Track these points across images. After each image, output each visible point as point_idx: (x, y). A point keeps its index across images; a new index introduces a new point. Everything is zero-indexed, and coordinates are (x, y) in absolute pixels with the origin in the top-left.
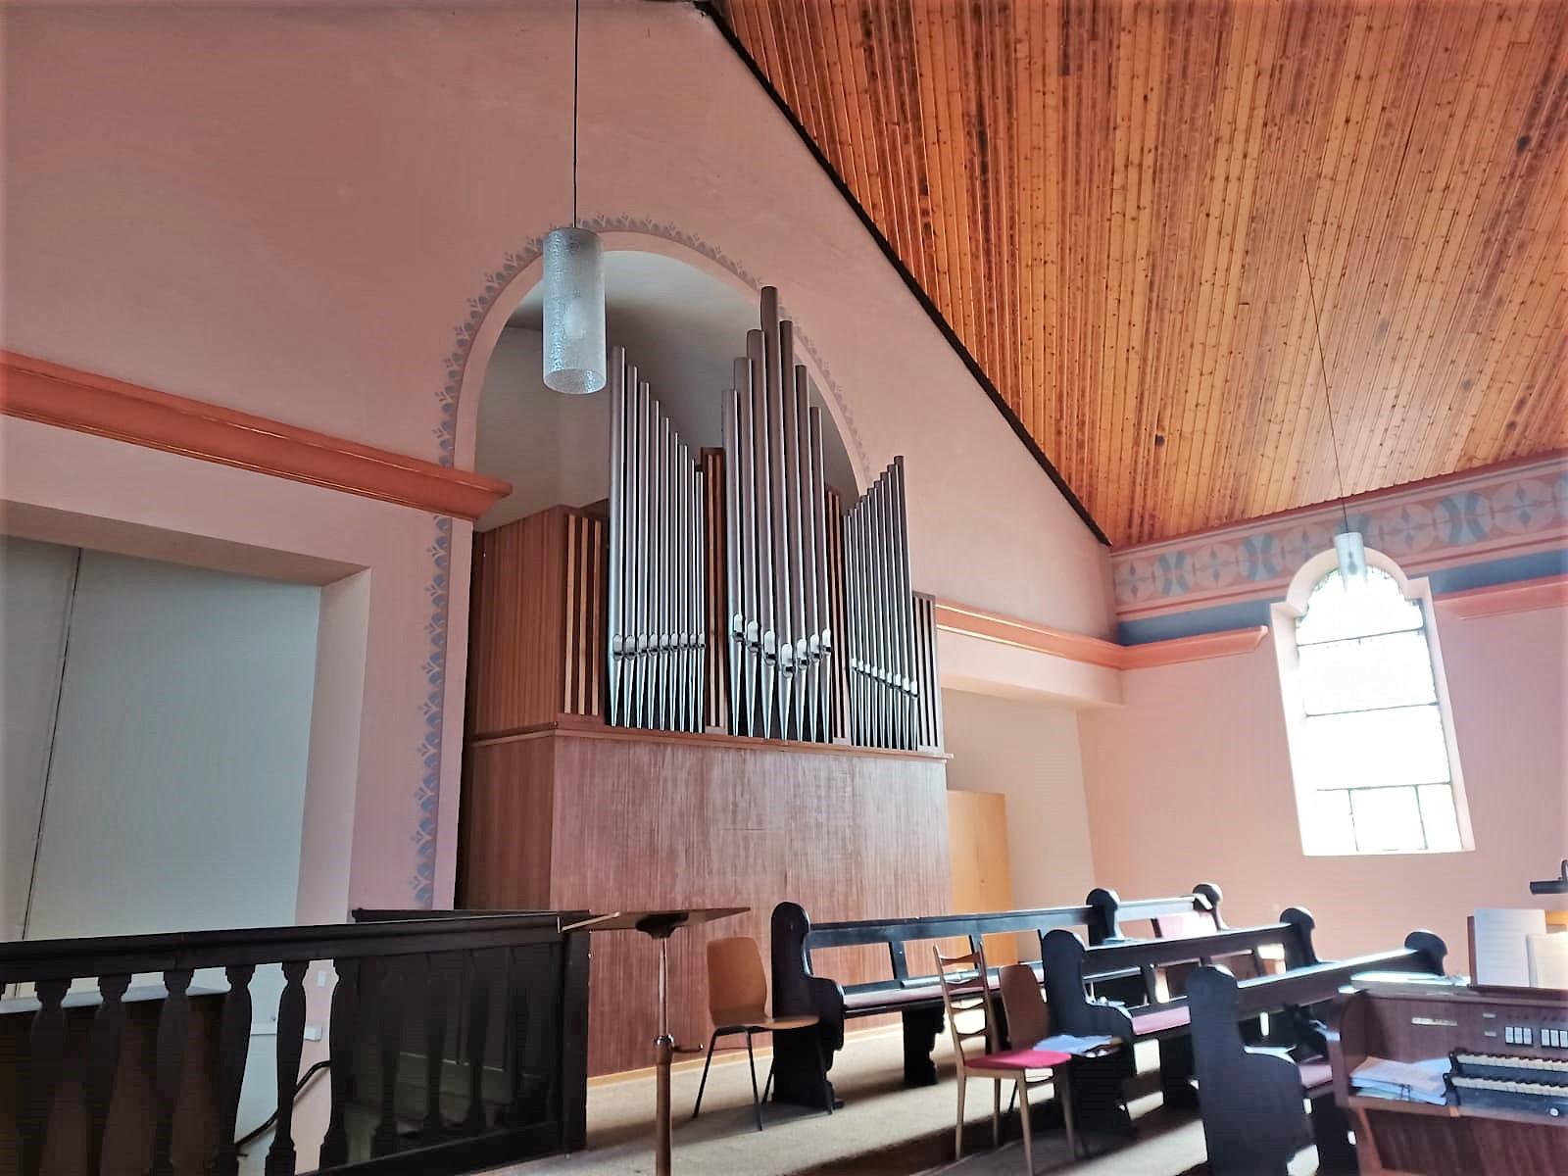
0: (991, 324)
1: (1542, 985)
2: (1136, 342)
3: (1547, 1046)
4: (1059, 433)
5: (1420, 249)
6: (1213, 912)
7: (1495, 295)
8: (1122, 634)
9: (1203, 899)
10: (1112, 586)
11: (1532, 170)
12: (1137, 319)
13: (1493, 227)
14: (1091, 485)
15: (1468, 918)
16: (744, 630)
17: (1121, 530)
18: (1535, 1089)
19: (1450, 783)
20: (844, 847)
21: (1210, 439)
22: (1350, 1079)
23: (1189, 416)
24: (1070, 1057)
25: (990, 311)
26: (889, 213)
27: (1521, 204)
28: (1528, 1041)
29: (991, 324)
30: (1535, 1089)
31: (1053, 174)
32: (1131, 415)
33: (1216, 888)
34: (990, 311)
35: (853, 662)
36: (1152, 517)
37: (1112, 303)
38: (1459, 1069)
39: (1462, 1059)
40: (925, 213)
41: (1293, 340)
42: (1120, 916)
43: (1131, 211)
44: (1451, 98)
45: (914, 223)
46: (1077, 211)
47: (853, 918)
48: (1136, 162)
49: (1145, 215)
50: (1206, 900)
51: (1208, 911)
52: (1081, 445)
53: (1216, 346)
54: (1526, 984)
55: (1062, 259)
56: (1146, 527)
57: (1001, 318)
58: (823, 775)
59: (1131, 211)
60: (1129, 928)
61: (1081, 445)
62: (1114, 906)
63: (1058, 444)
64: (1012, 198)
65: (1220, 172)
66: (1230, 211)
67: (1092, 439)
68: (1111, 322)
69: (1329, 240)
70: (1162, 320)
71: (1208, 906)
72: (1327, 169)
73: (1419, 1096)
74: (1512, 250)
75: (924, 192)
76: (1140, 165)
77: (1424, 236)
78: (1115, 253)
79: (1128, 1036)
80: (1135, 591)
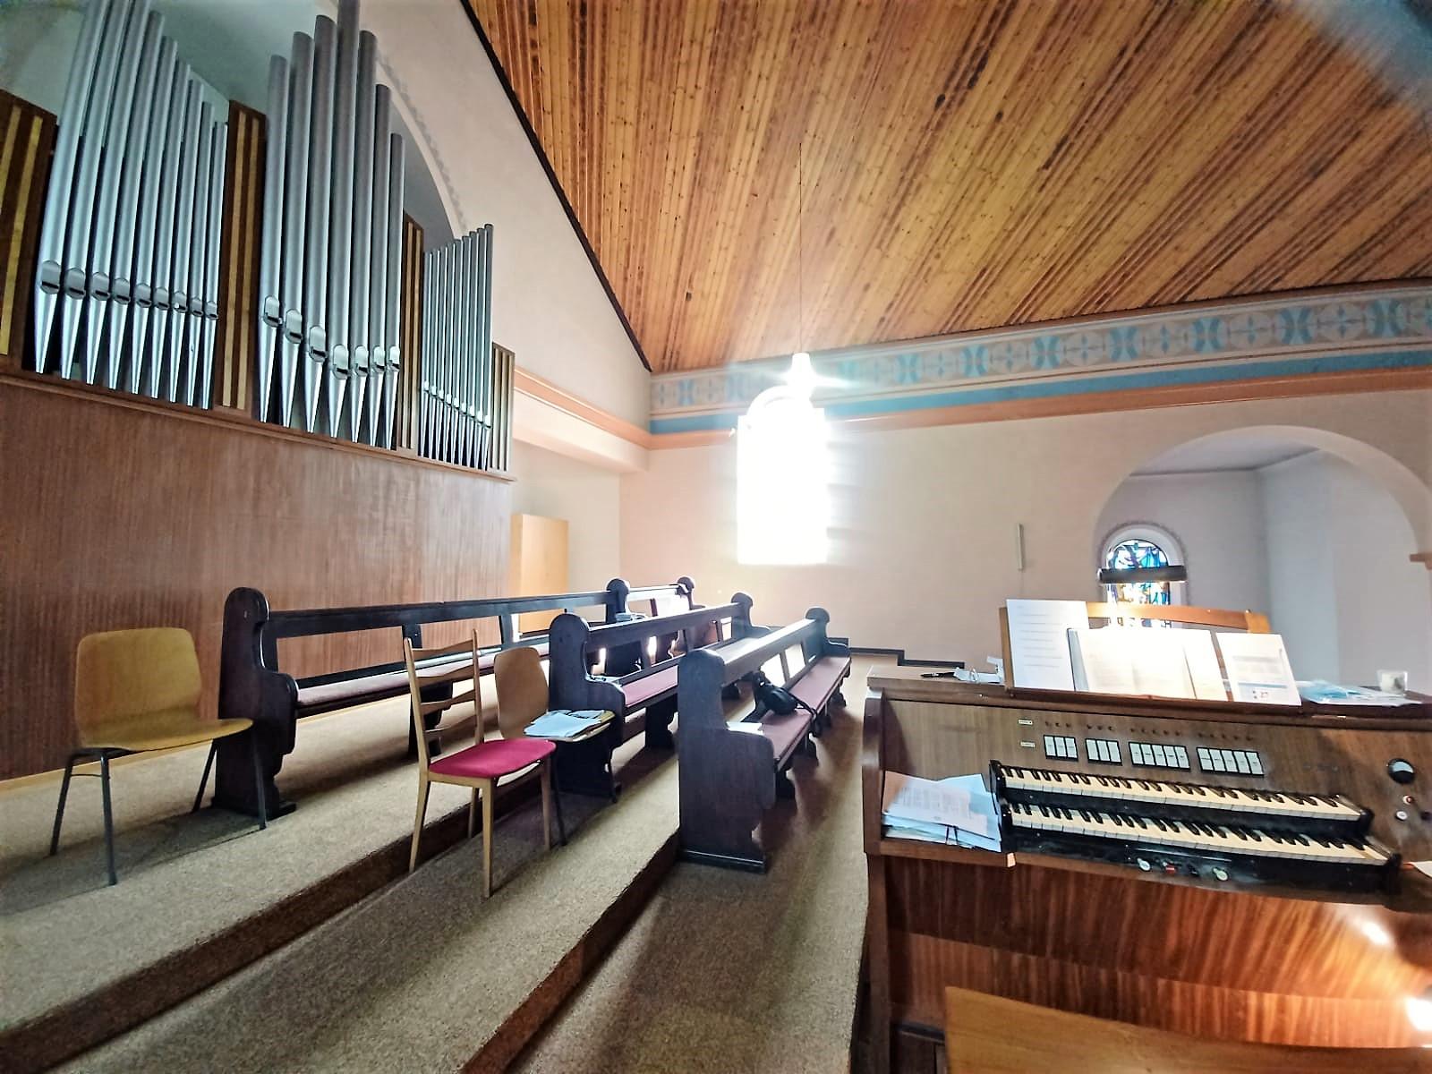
0: (583, 172)
1: (1094, 688)
2: (682, 212)
4: (626, 279)
5: (865, 173)
6: (689, 595)
7: (895, 225)
8: (654, 428)
9: (683, 586)
10: (651, 397)
11: (939, 125)
12: (685, 192)
13: (908, 168)
14: (643, 324)
15: (1242, 616)
16: (327, 348)
17: (658, 363)
18: (1108, 827)
20: (403, 541)
21: (719, 301)
23: (708, 281)
24: (554, 745)
25: (583, 160)
26: (503, 36)
27: (927, 152)
28: (1072, 754)
29: (583, 172)
30: (1108, 827)
31: (637, 36)
32: (673, 271)
33: (692, 580)
34: (583, 160)
35: (425, 385)
36: (678, 353)
37: (669, 173)
40: (534, 44)
41: (778, 232)
42: (630, 598)
43: (691, 89)
44: (909, 45)
45: (525, 55)
46: (651, 78)
47: (408, 600)
48: (699, 40)
49: (700, 96)
50: (684, 588)
52: (639, 292)
53: (732, 227)
54: (1066, 685)
55: (638, 122)
56: (674, 360)
57: (591, 169)
58: (382, 477)
59: (691, 89)
60: (635, 610)
61: (639, 292)
63: (625, 287)
64: (603, 49)
65: (755, 70)
66: (758, 106)
67: (647, 287)
68: (667, 191)
69: (815, 151)
70: (701, 196)
72: (825, 87)
73: (969, 841)
74: (913, 190)
75: (533, 21)
76: (702, 44)
77: (869, 165)
78: (675, 128)
79: (620, 710)
80: (662, 402)
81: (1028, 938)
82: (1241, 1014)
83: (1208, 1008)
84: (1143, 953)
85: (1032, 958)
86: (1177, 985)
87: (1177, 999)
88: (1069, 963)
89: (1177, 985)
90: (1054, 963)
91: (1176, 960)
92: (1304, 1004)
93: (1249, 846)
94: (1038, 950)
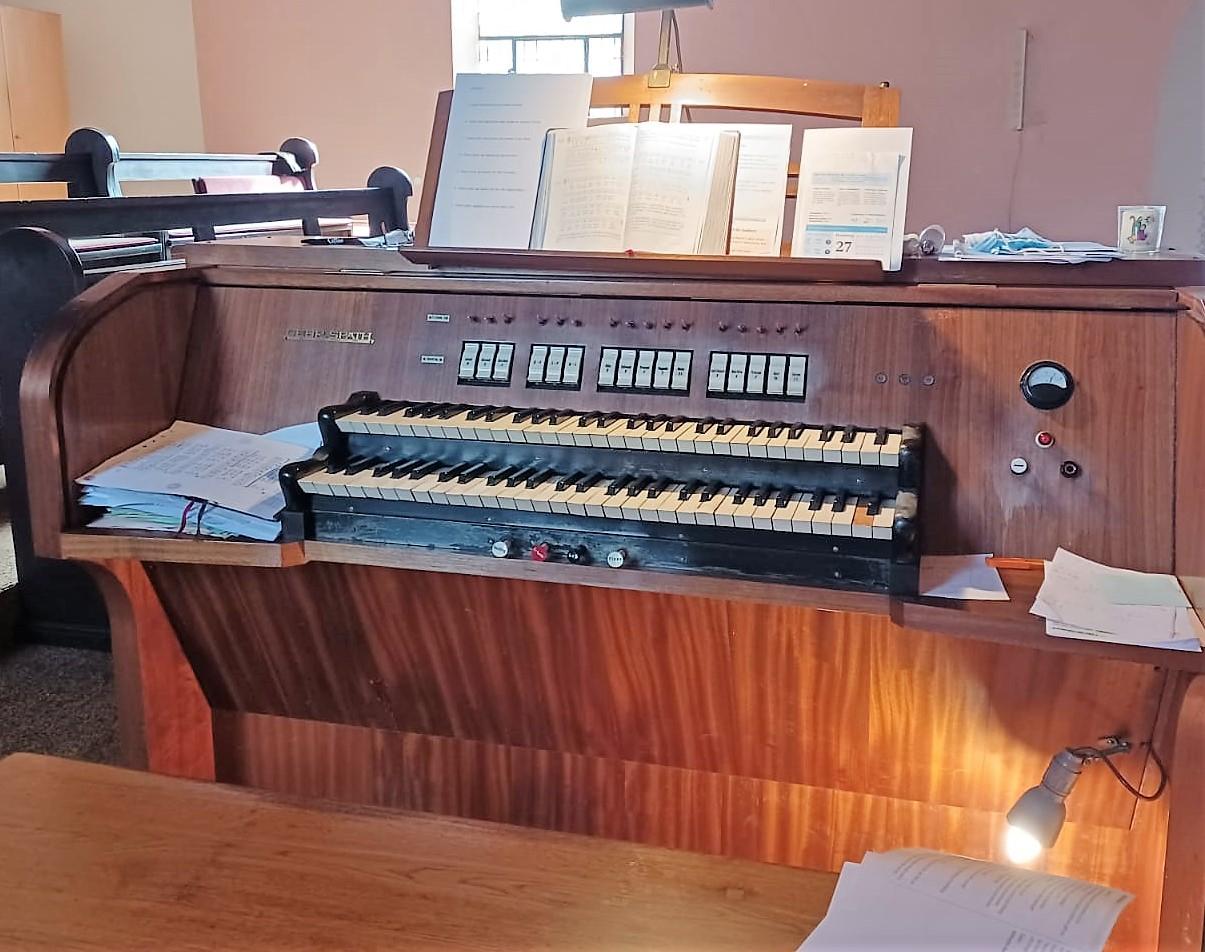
3: (646, 388)
9: (290, 159)
19: (621, 35)
22: (80, 491)
38: (339, 452)
39: (345, 423)
51: (297, 174)
62: (107, 156)
71: (296, 168)
81: (407, 705)
82: (752, 819)
83: (703, 804)
84: (589, 720)
85: (435, 740)
86: (654, 769)
87: (653, 795)
88: (490, 746)
89: (654, 769)
90: (469, 745)
91: (640, 726)
92: (859, 804)
93: (694, 509)
94: (440, 726)
